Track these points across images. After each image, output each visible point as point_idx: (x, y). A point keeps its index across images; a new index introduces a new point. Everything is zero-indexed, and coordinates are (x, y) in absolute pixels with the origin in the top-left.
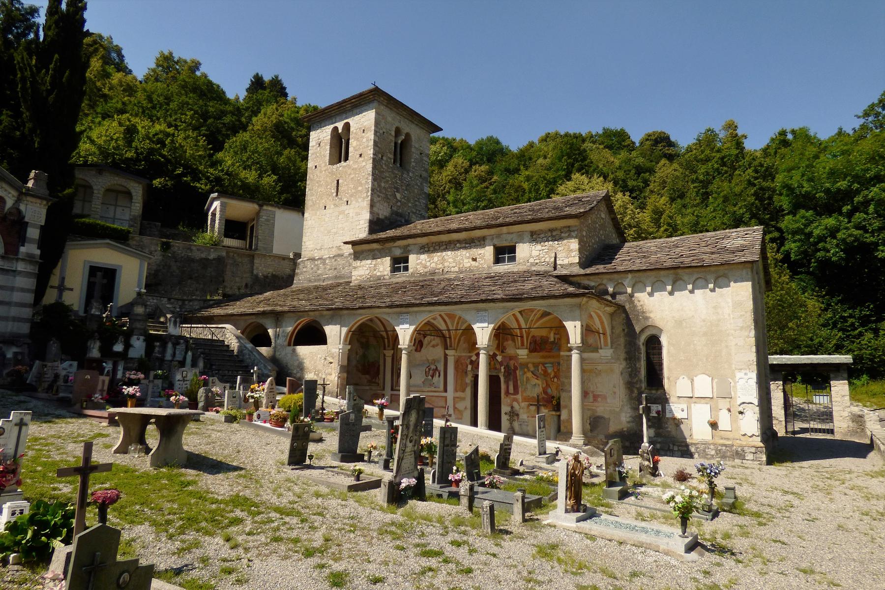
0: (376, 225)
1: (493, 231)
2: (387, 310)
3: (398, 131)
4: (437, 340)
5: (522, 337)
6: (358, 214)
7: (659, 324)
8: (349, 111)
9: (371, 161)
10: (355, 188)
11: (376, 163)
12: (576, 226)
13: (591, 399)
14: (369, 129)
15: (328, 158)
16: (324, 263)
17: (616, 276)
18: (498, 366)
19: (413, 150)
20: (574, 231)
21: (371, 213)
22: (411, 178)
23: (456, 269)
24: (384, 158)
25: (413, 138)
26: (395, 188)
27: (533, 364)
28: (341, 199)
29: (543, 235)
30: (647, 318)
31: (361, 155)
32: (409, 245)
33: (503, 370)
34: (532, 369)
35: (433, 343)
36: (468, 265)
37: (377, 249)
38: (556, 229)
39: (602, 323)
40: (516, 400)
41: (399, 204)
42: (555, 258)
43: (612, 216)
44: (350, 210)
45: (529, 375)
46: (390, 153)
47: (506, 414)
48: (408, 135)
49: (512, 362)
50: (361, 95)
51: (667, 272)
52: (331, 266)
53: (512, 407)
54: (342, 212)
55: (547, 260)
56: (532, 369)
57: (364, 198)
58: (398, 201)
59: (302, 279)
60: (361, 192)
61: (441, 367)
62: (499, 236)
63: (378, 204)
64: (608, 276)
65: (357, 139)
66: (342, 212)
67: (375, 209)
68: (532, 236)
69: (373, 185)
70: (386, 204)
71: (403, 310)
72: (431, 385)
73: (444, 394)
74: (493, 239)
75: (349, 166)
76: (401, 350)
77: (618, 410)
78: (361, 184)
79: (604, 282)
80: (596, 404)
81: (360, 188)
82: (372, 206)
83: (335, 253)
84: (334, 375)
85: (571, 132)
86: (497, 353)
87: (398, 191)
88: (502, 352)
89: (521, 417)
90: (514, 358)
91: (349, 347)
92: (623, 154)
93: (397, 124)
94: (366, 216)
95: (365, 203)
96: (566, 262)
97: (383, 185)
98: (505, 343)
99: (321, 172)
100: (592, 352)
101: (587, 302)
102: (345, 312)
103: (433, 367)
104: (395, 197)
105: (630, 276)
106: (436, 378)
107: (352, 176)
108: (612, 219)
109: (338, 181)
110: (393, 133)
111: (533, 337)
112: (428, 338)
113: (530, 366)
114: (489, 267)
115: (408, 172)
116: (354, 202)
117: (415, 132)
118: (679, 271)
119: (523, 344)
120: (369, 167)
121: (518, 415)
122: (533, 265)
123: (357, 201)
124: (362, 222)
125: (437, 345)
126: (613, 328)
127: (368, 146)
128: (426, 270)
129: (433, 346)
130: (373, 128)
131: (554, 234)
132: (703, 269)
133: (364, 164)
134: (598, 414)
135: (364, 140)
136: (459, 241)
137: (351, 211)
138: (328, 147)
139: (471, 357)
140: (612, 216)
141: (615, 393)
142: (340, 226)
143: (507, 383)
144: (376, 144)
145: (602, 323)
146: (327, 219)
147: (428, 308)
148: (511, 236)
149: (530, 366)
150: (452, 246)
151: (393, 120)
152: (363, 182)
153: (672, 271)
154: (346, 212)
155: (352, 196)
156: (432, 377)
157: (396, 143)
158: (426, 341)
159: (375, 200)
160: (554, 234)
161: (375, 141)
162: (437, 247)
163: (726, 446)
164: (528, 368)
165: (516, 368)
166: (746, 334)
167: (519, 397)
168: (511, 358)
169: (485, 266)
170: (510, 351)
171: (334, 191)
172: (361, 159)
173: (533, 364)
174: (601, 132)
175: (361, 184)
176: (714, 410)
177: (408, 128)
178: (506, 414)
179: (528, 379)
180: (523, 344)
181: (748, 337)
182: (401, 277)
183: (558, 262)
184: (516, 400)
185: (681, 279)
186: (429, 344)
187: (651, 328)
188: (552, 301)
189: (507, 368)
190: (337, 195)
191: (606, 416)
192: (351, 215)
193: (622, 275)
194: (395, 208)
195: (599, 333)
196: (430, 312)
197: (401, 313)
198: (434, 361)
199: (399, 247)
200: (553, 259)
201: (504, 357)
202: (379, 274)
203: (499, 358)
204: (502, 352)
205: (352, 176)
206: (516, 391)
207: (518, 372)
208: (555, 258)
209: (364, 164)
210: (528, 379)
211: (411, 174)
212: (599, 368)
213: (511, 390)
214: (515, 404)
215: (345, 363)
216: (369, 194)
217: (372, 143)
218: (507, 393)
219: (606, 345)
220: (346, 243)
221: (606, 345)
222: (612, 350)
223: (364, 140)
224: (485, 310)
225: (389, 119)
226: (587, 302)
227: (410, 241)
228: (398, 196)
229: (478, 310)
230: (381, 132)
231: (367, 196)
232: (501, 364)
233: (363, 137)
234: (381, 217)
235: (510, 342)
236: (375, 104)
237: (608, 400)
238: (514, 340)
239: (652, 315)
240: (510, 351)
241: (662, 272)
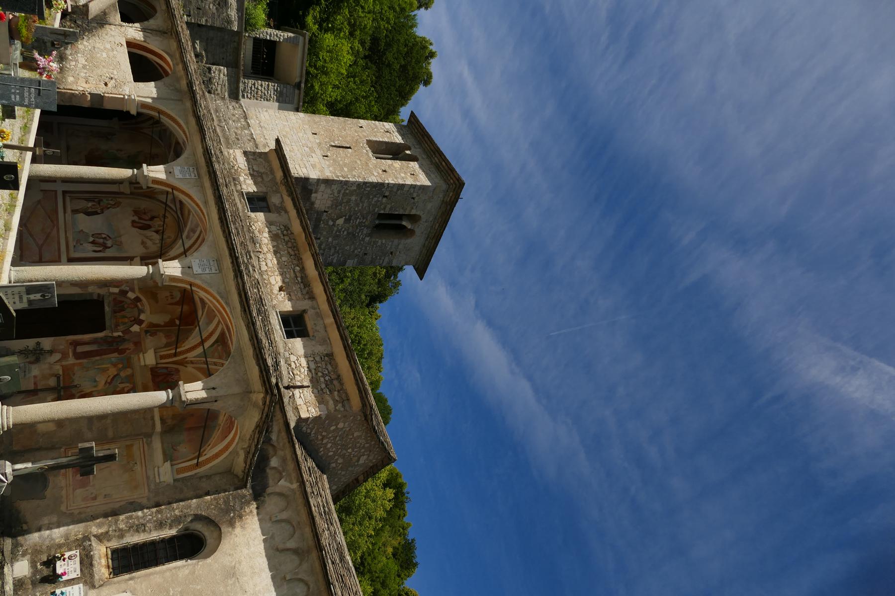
0: (302, 188)
2: (200, 150)
3: (414, 218)
5: (175, 355)
6: (314, 166)
7: (226, 545)
8: (431, 161)
9: (380, 181)
10: (345, 165)
11: (379, 187)
12: (351, 407)
14: (416, 180)
15: (374, 139)
16: (243, 128)
17: (291, 466)
18: (122, 327)
19: (396, 241)
20: (343, 406)
21: (318, 180)
22: (363, 239)
23: (264, 268)
24: (385, 199)
25: (409, 241)
26: (350, 217)
27: (132, 375)
29: (330, 368)
30: (232, 524)
32: (286, 212)
33: (116, 334)
34: (122, 374)
35: (149, 243)
36: (273, 282)
38: (342, 384)
39: (217, 456)
40: (65, 356)
41: (331, 223)
42: (302, 387)
43: (361, 478)
44: (317, 158)
45: (112, 371)
46: (391, 209)
47: (38, 344)
48: (412, 232)
49: (131, 346)
50: (452, 170)
52: (241, 135)
55: (298, 378)
56: (122, 374)
58: (334, 221)
60: (342, 170)
62: (319, 315)
63: (329, 191)
64: (289, 456)
65: (401, 168)
66: (312, 150)
67: (322, 187)
68: (327, 355)
69: (354, 183)
70: (329, 203)
71: (204, 170)
72: (78, 241)
74: (314, 308)
76: (139, 167)
77: (63, 508)
79: (280, 453)
81: (346, 169)
82: (327, 182)
83: (258, 141)
86: (143, 325)
87: (347, 221)
89: (33, 366)
90: (139, 346)
91: (133, 112)
92: (394, 567)
93: (424, 217)
94: (314, 175)
95: (328, 173)
96: (299, 402)
97: (353, 198)
98: (161, 334)
99: (356, 131)
101: (255, 405)
102: (188, 104)
103: (109, 243)
104: (339, 217)
105: (295, 486)
106: (91, 247)
107: (359, 162)
108: (357, 480)
109: (350, 148)
110: (413, 212)
111: (178, 371)
113: (129, 372)
114: (274, 307)
115: (369, 235)
116: (327, 163)
117: (416, 243)
118: (314, 555)
119: (162, 357)
120: (373, 179)
121: (37, 360)
122: (287, 361)
123: (329, 166)
124: (304, 170)
125: (146, 248)
126: (208, 477)
127: (396, 178)
128: (256, 232)
129: (143, 243)
130: (418, 184)
131: (335, 382)
132: (323, 587)
133: (376, 174)
135: (403, 175)
136: (303, 269)
137: (317, 160)
139: (133, 290)
140: (361, 478)
141: (95, 498)
142: (295, 147)
144: (402, 186)
145: (217, 456)
146: (301, 135)
147: (209, 192)
149: (129, 372)
151: (427, 210)
152: (354, 173)
154: (313, 155)
155: (334, 160)
156: (93, 242)
157: (400, 217)
159: (334, 187)
160: (335, 382)
161: (403, 185)
162: (290, 245)
164: (124, 368)
165: (121, 352)
167: (71, 360)
168: (138, 344)
169: (275, 302)
171: (337, 143)
172: (380, 171)
173: (132, 375)
174: (410, 538)
177: (421, 230)
178: (38, 344)
179: (105, 370)
180: (162, 357)
182: (242, 205)
183: (297, 392)
184: (65, 356)
185: (301, 561)
187: (216, 534)
188: (249, 352)
191: (48, 493)
192: (311, 159)
193: (294, 475)
194: (324, 216)
195: (198, 457)
196: (206, 203)
197: (197, 168)
198: (119, 245)
199: (283, 201)
200: (299, 384)
201: (138, 334)
202: (242, 179)
203: (136, 328)
204: (146, 332)
207: (116, 355)
208: (302, 387)
209: (376, 174)
210: (106, 370)
211: (367, 239)
212: (138, 468)
213: (80, 349)
214: (57, 356)
215: (108, 106)
216: (341, 179)
217: (401, 182)
218: (75, 344)
219: (179, 471)
220: (278, 141)
221: (179, 471)
223: (403, 175)
224: (220, 270)
225: (429, 206)
226: (255, 405)
228: (340, 221)
229: (218, 261)
230: (415, 195)
231: (338, 177)
232: (127, 331)
233: (405, 173)
234: (313, 195)
236: (444, 187)
237: (78, 491)
238: (167, 345)
239: (238, 530)
240: (149, 342)
241: (307, 530)
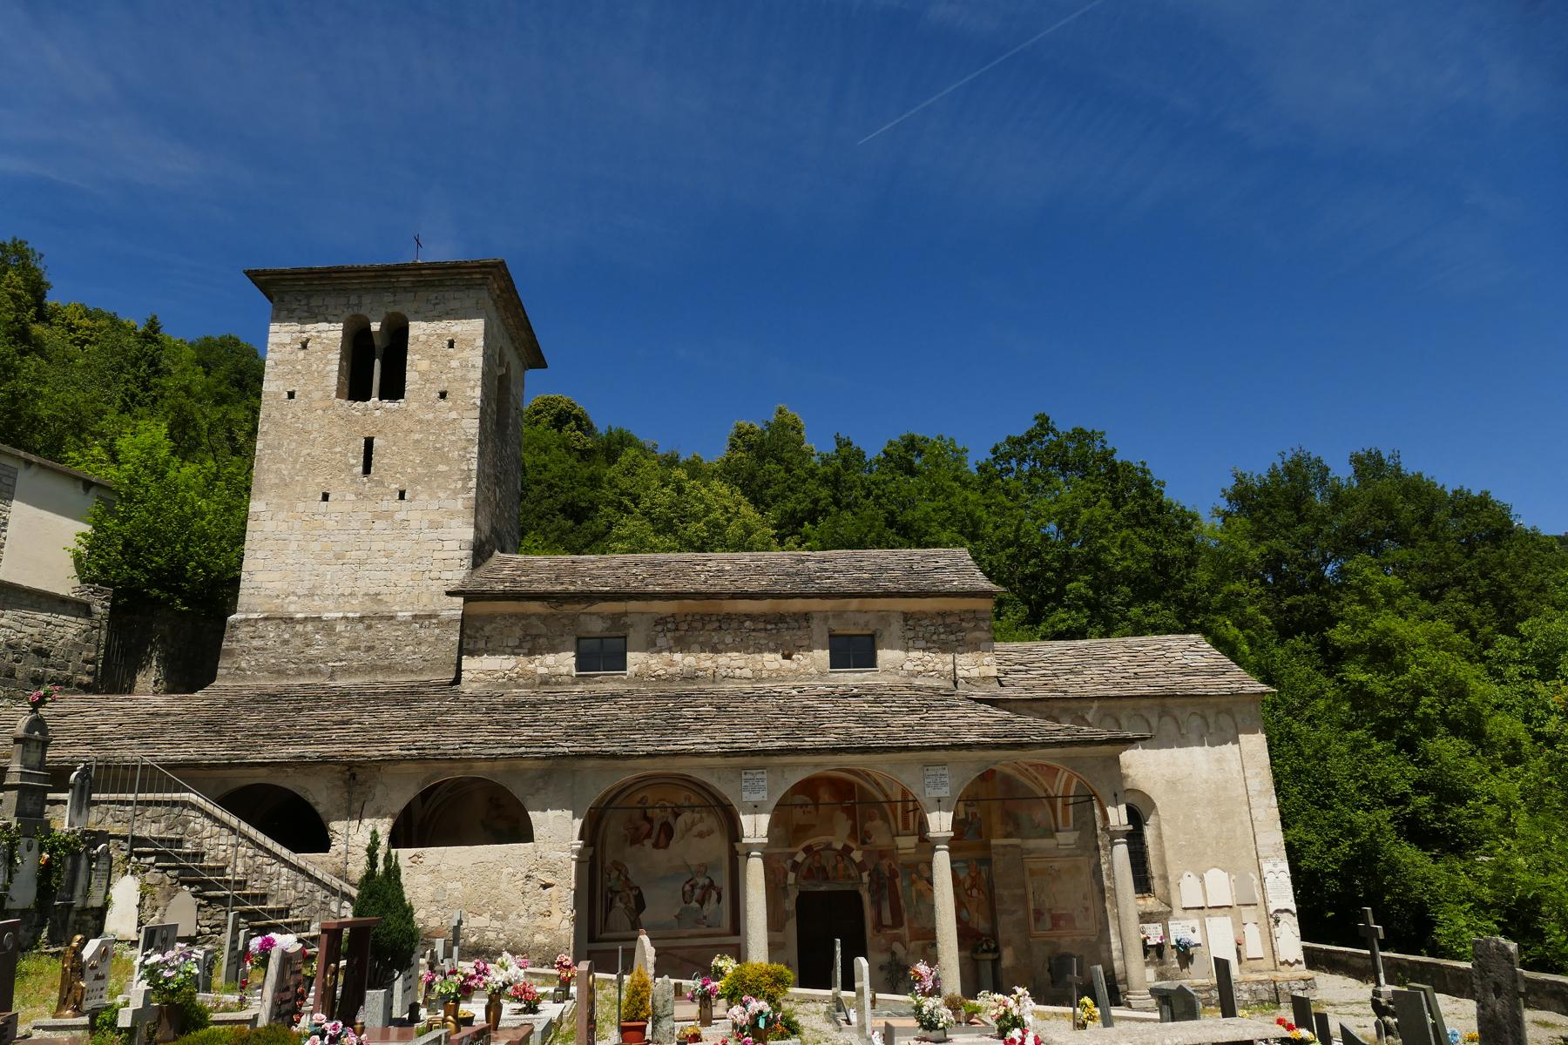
1: (829, 604)
2: (719, 761)
4: (709, 821)
8: (405, 289)
12: (985, 612)
13: (1048, 924)
18: (853, 872)
28: (380, 483)
29: (926, 622)
31: (443, 395)
32: (626, 614)
37: (538, 616)
38: (951, 614)
40: (899, 939)
49: (885, 862)
51: (1151, 701)
53: (893, 954)
54: (387, 515)
57: (455, 492)
59: (246, 665)
60: (446, 476)
61: (723, 880)
66: (387, 515)
68: (906, 620)
72: (698, 922)
73: (733, 940)
75: (407, 415)
77: (1094, 939)
78: (445, 459)
80: (1059, 932)
84: (556, 918)
85: (216, 336)
86: (853, 845)
88: (864, 843)
100: (1042, 837)
103: (702, 881)
106: (710, 907)
109: (369, 443)
112: (686, 817)
118: (1168, 701)
125: (710, 832)
128: (672, 670)
129: (701, 835)
131: (948, 621)
133: (454, 415)
134: (1062, 950)
135: (454, 364)
138: (335, 357)
139: (793, 855)
141: (1087, 909)
143: (877, 905)
148: (867, 617)
150: (735, 625)
153: (1157, 701)
156: (702, 902)
158: (680, 824)
160: (948, 621)
163: (1259, 982)
165: (894, 874)
166: (1266, 802)
167: (904, 931)
168: (882, 854)
170: (880, 840)
172: (442, 402)
175: (445, 459)
176: (1240, 924)
181: (1269, 806)
184: (899, 939)
186: (688, 830)
189: (876, 875)
190: (367, 470)
192: (414, 524)
197: (745, 768)
198: (704, 869)
199: (599, 615)
201: (867, 853)
203: (857, 856)
204: (864, 843)
205: (417, 436)
206: (897, 921)
207: (898, 881)
212: (1056, 865)
213: (887, 917)
214: (897, 946)
216: (473, 483)
218: (879, 926)
222: (1077, 834)
227: (633, 606)
229: (928, 764)
232: (861, 867)
235: (878, 823)
238: (885, 819)
239: (1130, 772)
240: (880, 840)
